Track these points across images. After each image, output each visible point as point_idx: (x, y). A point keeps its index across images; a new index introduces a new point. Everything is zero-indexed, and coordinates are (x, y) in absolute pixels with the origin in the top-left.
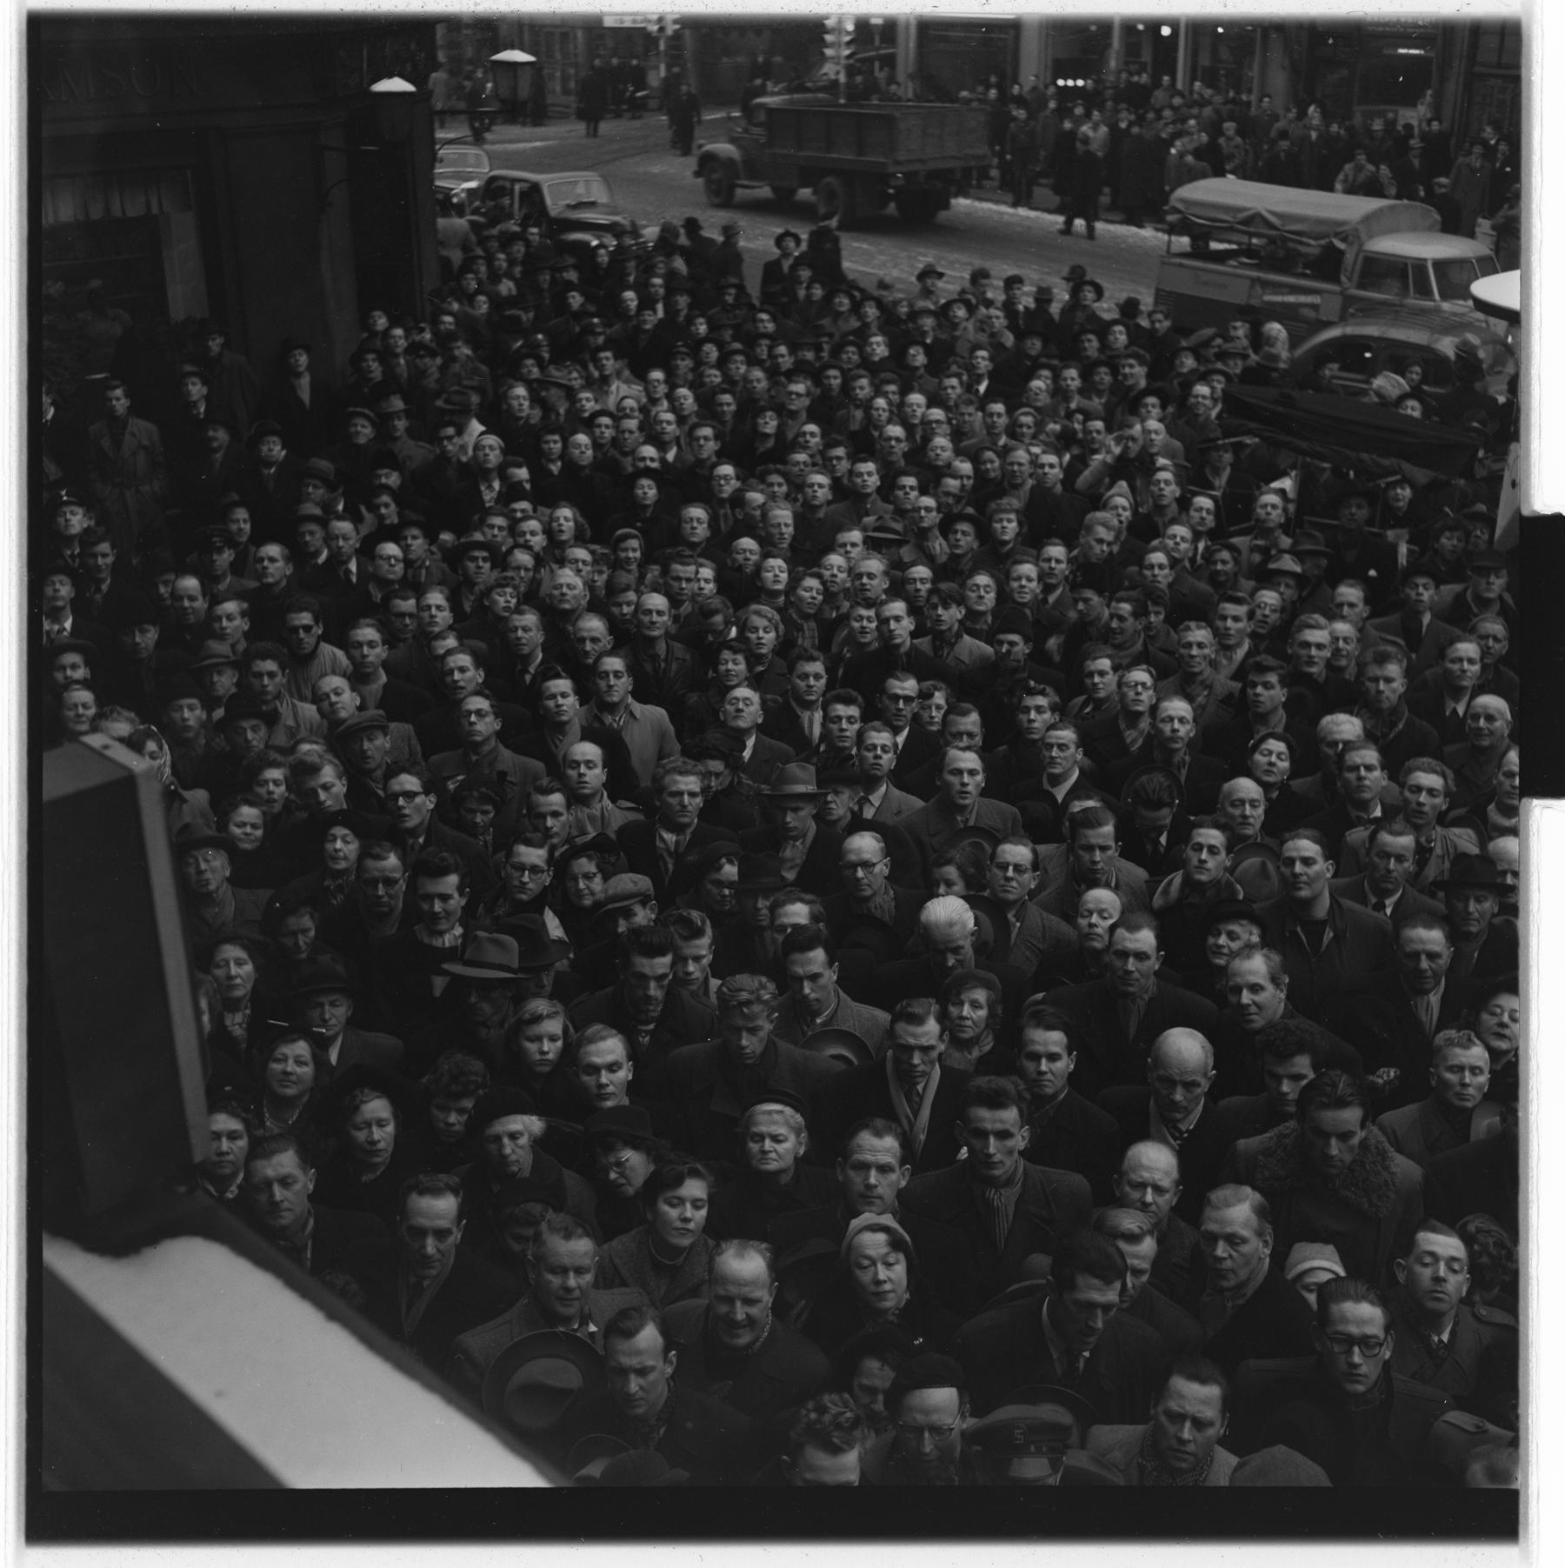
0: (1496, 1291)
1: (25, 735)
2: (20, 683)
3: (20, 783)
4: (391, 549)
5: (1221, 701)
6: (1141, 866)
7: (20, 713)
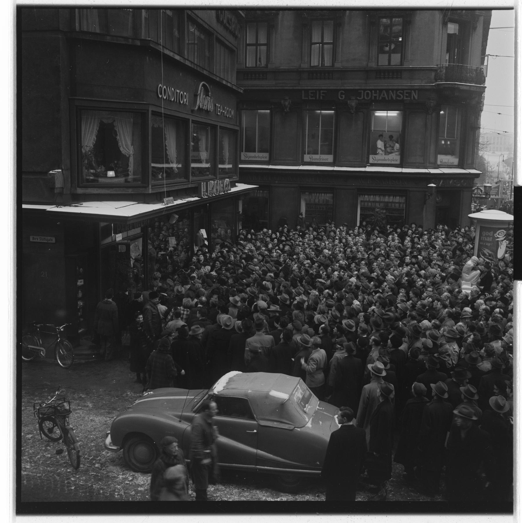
1: (15, 384)
7: (14, 305)
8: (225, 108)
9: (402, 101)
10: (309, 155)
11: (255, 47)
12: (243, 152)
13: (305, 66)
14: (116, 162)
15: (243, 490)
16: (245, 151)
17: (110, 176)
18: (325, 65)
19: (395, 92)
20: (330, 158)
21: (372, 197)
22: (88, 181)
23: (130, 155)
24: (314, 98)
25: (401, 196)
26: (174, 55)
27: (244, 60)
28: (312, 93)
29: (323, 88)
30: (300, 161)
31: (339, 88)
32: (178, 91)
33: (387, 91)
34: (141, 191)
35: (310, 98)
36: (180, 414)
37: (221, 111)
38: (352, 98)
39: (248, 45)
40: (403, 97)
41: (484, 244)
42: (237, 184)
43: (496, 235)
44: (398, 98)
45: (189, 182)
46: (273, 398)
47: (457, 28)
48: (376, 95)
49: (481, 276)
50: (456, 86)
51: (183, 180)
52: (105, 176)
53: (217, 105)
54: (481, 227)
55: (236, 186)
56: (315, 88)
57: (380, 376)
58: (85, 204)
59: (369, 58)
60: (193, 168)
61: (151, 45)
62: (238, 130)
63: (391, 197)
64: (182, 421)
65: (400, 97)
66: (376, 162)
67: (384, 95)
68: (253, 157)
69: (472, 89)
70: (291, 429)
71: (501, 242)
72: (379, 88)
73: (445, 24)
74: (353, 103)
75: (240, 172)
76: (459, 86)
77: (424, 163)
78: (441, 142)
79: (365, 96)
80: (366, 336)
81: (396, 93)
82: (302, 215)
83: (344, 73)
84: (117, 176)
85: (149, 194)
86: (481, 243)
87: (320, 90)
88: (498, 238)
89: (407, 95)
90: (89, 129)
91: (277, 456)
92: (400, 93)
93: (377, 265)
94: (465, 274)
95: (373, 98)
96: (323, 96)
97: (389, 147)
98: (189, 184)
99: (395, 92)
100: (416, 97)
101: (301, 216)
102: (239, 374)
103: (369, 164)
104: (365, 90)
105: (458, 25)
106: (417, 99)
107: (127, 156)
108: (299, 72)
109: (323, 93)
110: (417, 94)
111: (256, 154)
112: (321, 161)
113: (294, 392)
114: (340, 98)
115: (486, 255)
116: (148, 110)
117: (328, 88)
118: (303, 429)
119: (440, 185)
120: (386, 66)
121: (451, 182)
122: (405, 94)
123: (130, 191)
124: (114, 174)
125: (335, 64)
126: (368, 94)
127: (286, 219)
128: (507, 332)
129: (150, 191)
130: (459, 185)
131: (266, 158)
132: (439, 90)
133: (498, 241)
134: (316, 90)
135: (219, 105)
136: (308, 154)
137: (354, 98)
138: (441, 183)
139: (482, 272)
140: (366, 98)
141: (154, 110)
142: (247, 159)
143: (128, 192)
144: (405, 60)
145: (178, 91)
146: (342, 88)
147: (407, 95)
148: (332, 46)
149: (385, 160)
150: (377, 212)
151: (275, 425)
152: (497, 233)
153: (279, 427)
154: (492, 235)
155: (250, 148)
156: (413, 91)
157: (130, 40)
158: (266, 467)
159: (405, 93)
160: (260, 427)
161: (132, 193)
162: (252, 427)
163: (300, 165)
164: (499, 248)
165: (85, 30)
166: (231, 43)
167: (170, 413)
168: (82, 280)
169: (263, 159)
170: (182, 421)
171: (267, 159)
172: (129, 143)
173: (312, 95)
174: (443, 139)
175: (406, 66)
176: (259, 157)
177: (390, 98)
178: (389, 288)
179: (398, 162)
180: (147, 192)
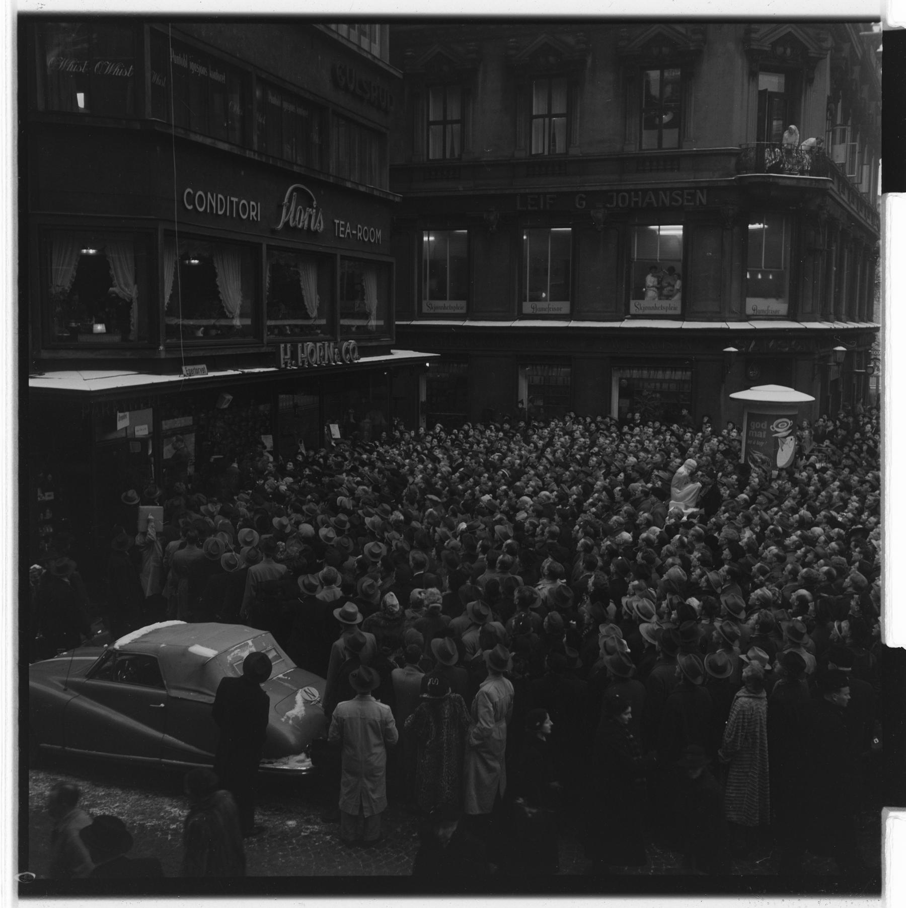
0: (556, 541)
2: (13, 56)
3: (14, 218)
4: (521, 515)
6: (882, 91)
11: (441, 127)
18: (557, 152)
20: (564, 307)
23: (132, 300)
24: (536, 208)
30: (516, 313)
33: (656, 191)
35: (529, 208)
36: (65, 679)
37: (348, 231)
39: (430, 123)
41: (754, 443)
42: (392, 351)
43: (773, 428)
46: (194, 655)
47: (783, 80)
48: (637, 199)
49: (703, 492)
53: (337, 221)
55: (392, 354)
57: (354, 625)
58: (47, 375)
60: (342, 326)
63: (668, 373)
64: (69, 689)
65: (677, 201)
66: (641, 312)
67: (650, 199)
71: (783, 440)
73: (753, 76)
78: (757, 275)
79: (620, 202)
82: (522, 402)
86: (750, 442)
88: (777, 432)
89: (689, 197)
92: (677, 195)
93: (550, 477)
94: (675, 489)
95: (633, 205)
97: (668, 286)
98: (263, 346)
100: (704, 201)
101: (520, 406)
102: (179, 625)
103: (629, 316)
105: (784, 75)
106: (705, 204)
110: (705, 196)
111: (447, 303)
112: (551, 312)
114: (578, 206)
115: (757, 461)
119: (750, 350)
121: (771, 344)
123: (128, 355)
124: (104, 328)
126: (623, 197)
128: (665, 573)
130: (787, 349)
133: (777, 438)
135: (342, 222)
136: (530, 300)
139: (704, 484)
142: (432, 311)
145: (235, 199)
148: (564, 119)
149: (655, 308)
151: (192, 696)
153: (195, 700)
154: (765, 427)
156: (698, 191)
158: (174, 761)
160: (170, 700)
161: (132, 357)
162: (158, 699)
164: (780, 449)
169: (457, 311)
171: (464, 311)
172: (131, 282)
174: (759, 272)
175: (686, 149)
179: (678, 312)
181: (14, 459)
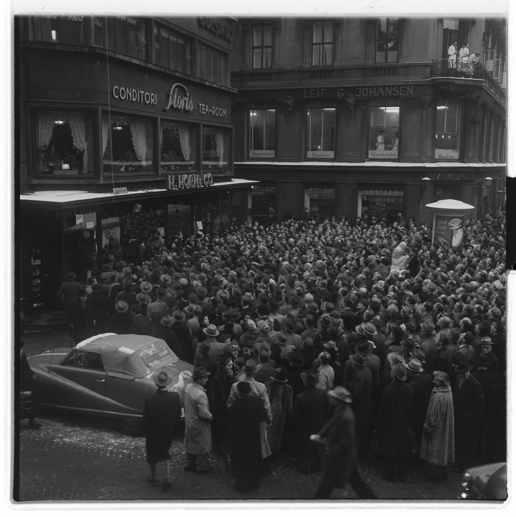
5: (187, 469)
8: (213, 107)
9: (398, 97)
10: (312, 152)
12: (251, 149)
13: (306, 66)
14: (70, 156)
15: (95, 432)
16: (254, 149)
17: (65, 169)
19: (391, 88)
20: (331, 154)
21: (371, 191)
22: (44, 173)
23: (84, 150)
24: (315, 97)
25: (400, 190)
26: (130, 60)
27: (251, 63)
28: (313, 92)
29: (323, 86)
30: (303, 158)
31: (337, 86)
32: (142, 92)
33: (384, 87)
34: (93, 181)
35: (311, 97)
36: (49, 365)
38: (350, 96)
39: (254, 48)
40: (399, 94)
42: (232, 179)
43: (450, 224)
44: (394, 94)
45: (158, 175)
48: (373, 92)
50: (450, 81)
51: (151, 173)
52: (60, 168)
53: (200, 105)
54: (437, 217)
56: (315, 87)
58: (36, 193)
59: (366, 54)
61: (97, 51)
62: (232, 129)
63: (390, 192)
65: (396, 93)
66: (375, 157)
67: (381, 92)
68: (260, 154)
69: (468, 83)
70: (131, 379)
71: (456, 231)
72: (376, 85)
74: (351, 100)
75: (235, 169)
76: (454, 81)
77: (420, 158)
80: (248, 307)
81: (392, 89)
83: (342, 71)
84: (71, 168)
85: (101, 185)
86: (437, 232)
87: (320, 89)
88: (452, 226)
89: (403, 91)
90: (45, 126)
91: (120, 402)
92: (396, 89)
93: (323, 252)
95: (370, 95)
96: (323, 94)
98: (159, 177)
99: (391, 88)
100: (412, 93)
103: (368, 160)
104: (362, 87)
107: (82, 151)
108: (301, 72)
109: (323, 91)
110: (412, 90)
111: (264, 151)
113: (143, 349)
114: (339, 96)
116: (98, 110)
117: (328, 86)
118: (142, 379)
119: (437, 179)
120: (384, 63)
121: (449, 176)
122: (401, 90)
123: (82, 182)
125: (335, 63)
126: (365, 91)
127: (290, 213)
129: (102, 182)
130: (459, 178)
131: (272, 155)
132: (434, 85)
133: (452, 230)
134: (317, 89)
136: (312, 150)
137: (353, 96)
138: (438, 177)
140: (363, 95)
141: (113, 110)
142: (255, 156)
143: (80, 182)
144: (401, 57)
145: (142, 92)
146: (341, 86)
147: (403, 91)
149: (383, 155)
150: (377, 206)
151: (120, 375)
152: (452, 221)
154: (446, 224)
155: (258, 146)
156: (408, 87)
157: (79, 48)
159: (401, 89)
160: (108, 378)
161: (85, 183)
163: (303, 162)
164: (454, 236)
165: (40, 40)
166: (222, 47)
167: (43, 366)
168: (40, 261)
169: (269, 156)
170: (51, 372)
171: (273, 156)
172: (84, 140)
173: (313, 94)
174: (443, 134)
176: (266, 154)
177: (387, 95)
178: (313, 272)
179: (396, 157)
180: (98, 183)
181: (12, 104)
